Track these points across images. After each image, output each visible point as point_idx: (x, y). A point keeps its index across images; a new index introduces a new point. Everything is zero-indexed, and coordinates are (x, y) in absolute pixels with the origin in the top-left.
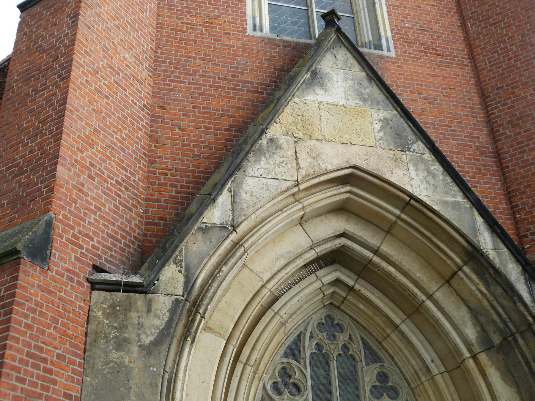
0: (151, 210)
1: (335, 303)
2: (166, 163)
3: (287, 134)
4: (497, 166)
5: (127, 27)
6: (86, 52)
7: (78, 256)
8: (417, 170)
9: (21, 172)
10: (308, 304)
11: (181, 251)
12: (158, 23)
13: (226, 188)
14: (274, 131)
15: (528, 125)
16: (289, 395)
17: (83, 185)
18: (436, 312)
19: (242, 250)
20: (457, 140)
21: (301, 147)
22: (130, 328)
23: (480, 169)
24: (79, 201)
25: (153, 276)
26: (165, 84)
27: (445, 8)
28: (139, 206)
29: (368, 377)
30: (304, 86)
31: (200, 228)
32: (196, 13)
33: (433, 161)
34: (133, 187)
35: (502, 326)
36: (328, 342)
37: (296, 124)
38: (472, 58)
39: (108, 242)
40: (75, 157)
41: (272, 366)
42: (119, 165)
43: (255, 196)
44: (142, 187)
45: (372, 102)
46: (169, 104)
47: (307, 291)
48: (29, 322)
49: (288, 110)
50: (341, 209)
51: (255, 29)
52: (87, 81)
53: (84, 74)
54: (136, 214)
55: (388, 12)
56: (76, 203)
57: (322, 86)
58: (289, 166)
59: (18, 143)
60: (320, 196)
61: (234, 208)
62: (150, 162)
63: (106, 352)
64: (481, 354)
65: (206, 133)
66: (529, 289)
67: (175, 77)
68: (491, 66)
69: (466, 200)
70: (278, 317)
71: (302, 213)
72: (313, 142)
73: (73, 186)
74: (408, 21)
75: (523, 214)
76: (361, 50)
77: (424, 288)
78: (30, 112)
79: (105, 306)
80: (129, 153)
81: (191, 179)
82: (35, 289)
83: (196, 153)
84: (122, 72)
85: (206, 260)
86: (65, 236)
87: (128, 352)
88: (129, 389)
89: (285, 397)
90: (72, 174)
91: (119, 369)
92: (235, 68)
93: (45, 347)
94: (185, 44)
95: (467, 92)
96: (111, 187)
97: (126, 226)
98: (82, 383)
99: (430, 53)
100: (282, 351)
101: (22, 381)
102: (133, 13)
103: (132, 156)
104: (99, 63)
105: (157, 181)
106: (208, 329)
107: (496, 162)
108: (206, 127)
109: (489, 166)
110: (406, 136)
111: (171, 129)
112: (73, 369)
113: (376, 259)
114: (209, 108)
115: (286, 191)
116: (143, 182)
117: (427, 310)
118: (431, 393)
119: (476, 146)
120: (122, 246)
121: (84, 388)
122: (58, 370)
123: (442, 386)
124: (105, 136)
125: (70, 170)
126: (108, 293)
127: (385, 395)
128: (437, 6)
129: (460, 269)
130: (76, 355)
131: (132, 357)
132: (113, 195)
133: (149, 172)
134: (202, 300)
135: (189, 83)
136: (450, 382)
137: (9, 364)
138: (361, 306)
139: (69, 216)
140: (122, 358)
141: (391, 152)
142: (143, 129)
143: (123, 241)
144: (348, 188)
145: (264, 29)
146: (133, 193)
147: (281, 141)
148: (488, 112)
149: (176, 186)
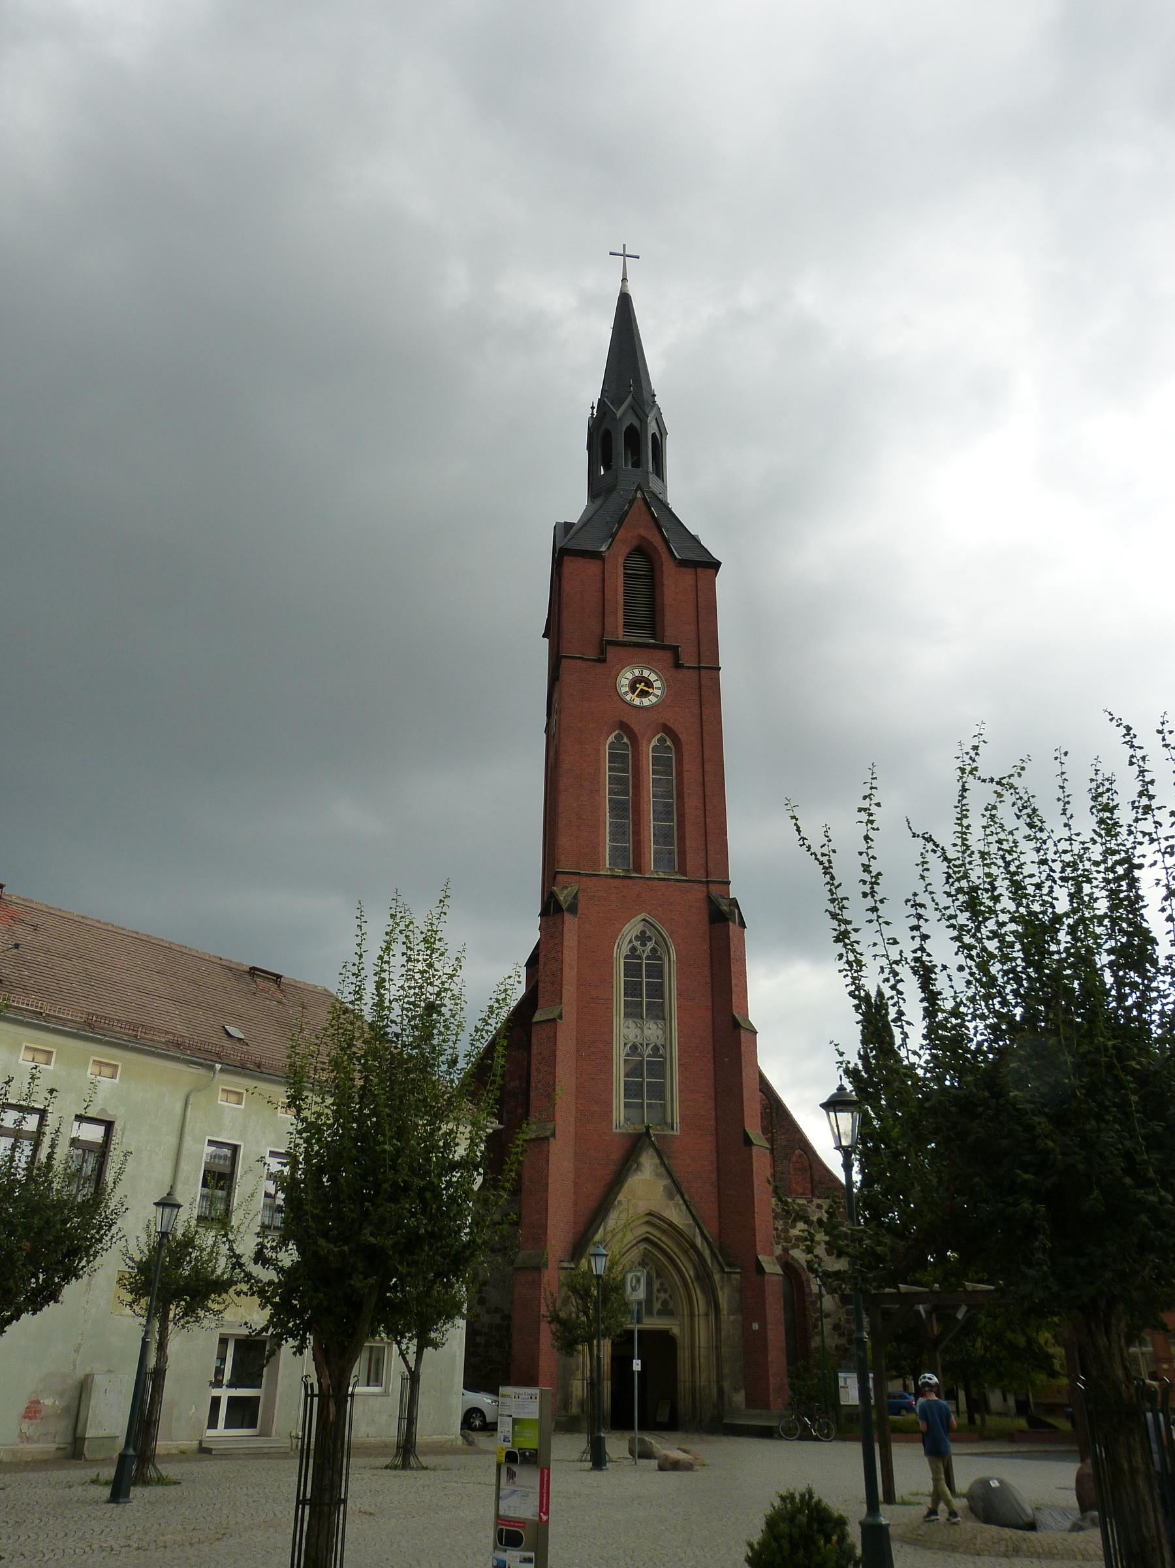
14: (620, 1197)
29: (656, 1286)
50: (647, 1223)
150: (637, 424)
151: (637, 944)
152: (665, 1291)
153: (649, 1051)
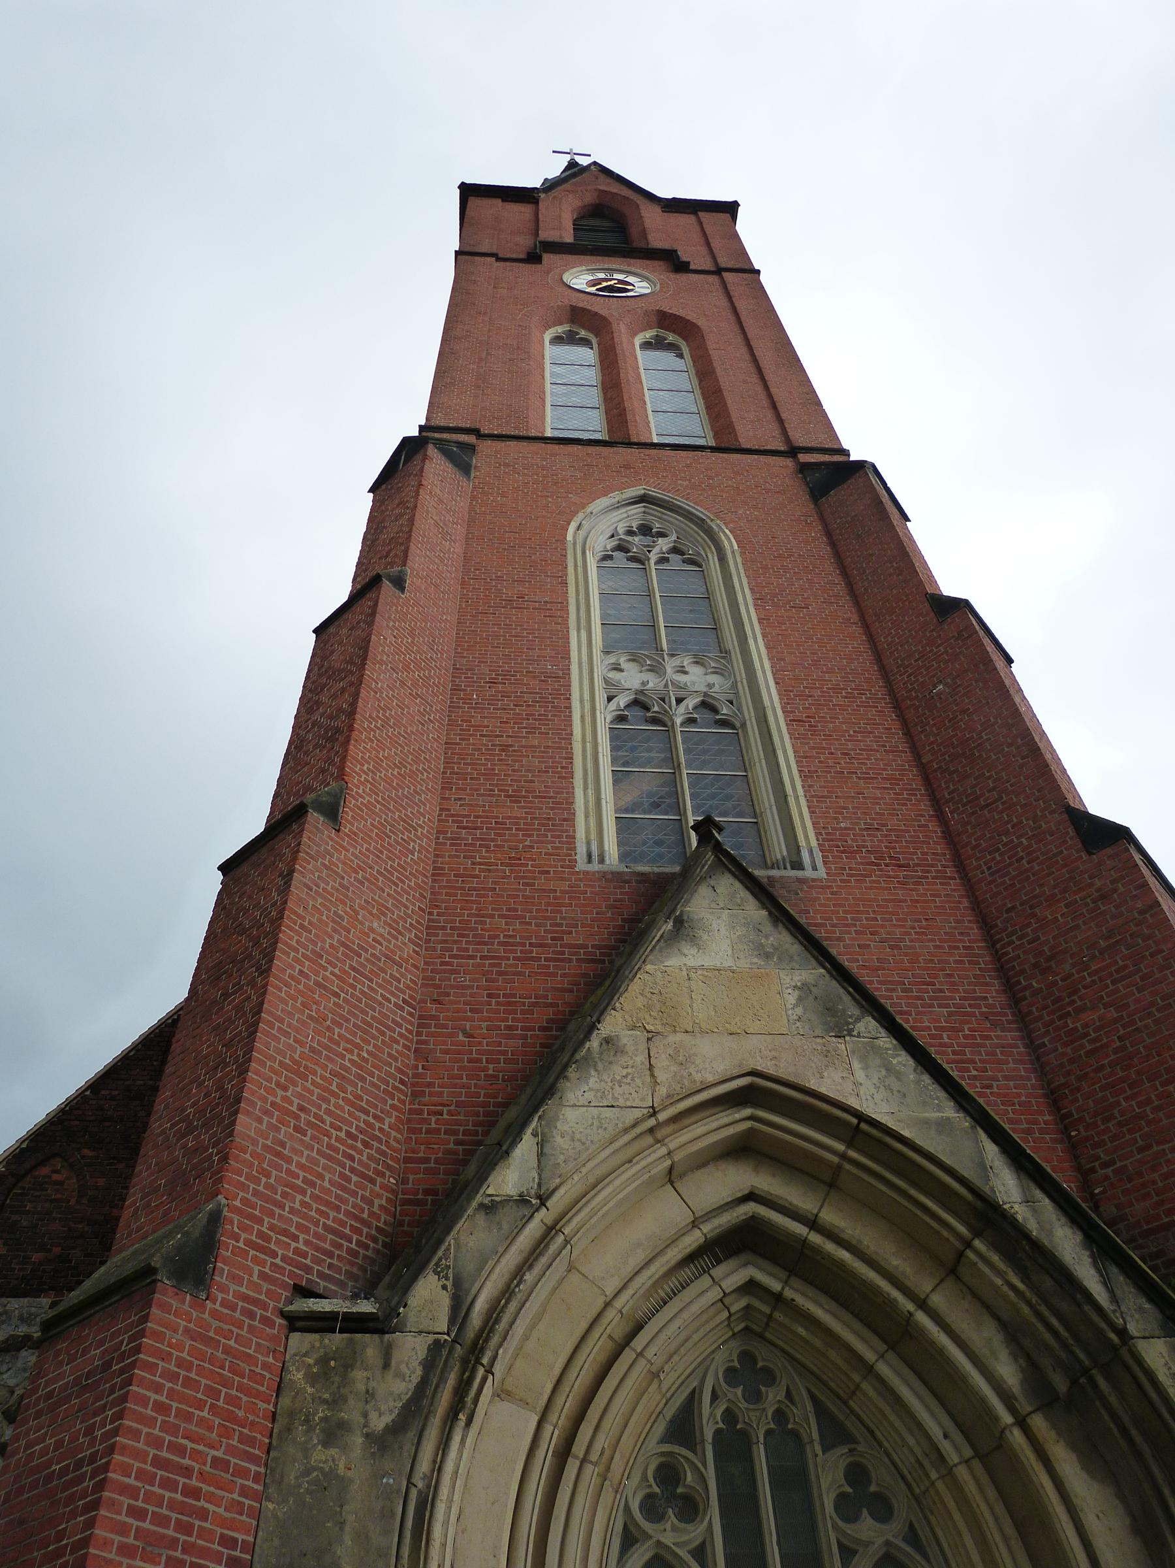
0: (411, 1177)
1: (754, 1327)
2: (441, 1094)
3: (633, 1028)
4: (1026, 1046)
5: (377, 880)
6: (302, 926)
7: (267, 1270)
8: (866, 1068)
9: (190, 1129)
10: (701, 1333)
11: (448, 1249)
12: (435, 868)
13: (529, 1131)
14: (612, 1024)
15: (1067, 967)
16: (675, 1521)
17: (283, 1145)
18: (936, 1334)
19: (560, 1239)
20: (947, 1006)
21: (658, 1046)
22: (351, 1402)
23: (994, 1054)
24: (274, 1172)
25: (396, 1299)
26: (442, 964)
27: (906, 789)
28: (388, 1173)
29: (828, 1477)
30: (662, 943)
31: (481, 1206)
32: (495, 846)
33: (895, 1049)
34: (380, 1141)
35: (1063, 1355)
36: (746, 1405)
37: (649, 1008)
38: (959, 863)
39: (325, 1241)
40: (271, 1098)
41: (639, 1460)
42: (352, 1105)
43: (579, 1140)
44: (395, 1139)
45: (779, 958)
46: (448, 995)
47: (696, 1308)
48: (163, 1399)
49: (635, 987)
51: (590, 860)
52: (301, 972)
53: (296, 960)
54: (382, 1187)
55: (809, 807)
56: (268, 1176)
57: (694, 940)
58: (638, 1081)
59: (192, 1082)
60: (699, 1129)
61: (543, 1164)
62: (415, 1095)
63: (306, 1451)
64: (1033, 1415)
65: (508, 1037)
66: (1101, 1275)
67: (459, 949)
68: (991, 874)
69: (961, 1115)
70: (642, 1362)
71: (669, 1162)
72: (679, 1037)
73: (266, 1148)
74: (844, 818)
75: (1082, 1130)
76: (758, 873)
77: (908, 1288)
78: (214, 1029)
79: (311, 1361)
80: (373, 1084)
81: (481, 1118)
82: (179, 1337)
83: (491, 1072)
84: (366, 951)
85: (490, 1263)
86: (244, 1236)
87: (345, 1449)
88: (342, 1524)
89: (668, 1526)
90: (264, 1127)
91: (329, 1484)
92: (557, 925)
93: (190, 1445)
94: (477, 896)
95: (957, 922)
96: (337, 1144)
97: (363, 1211)
98: (258, 1515)
99: (886, 865)
100: (660, 1429)
101: (140, 1514)
102: (389, 858)
103: (378, 1088)
104: (324, 941)
105: (424, 1127)
106: (502, 1394)
107: (1022, 1038)
108: (508, 1028)
109: (1011, 1046)
110: (844, 1011)
111: (451, 1035)
112: (242, 1486)
113: (815, 1238)
114: (514, 996)
115: (634, 1126)
116: (398, 1130)
117: (922, 1331)
118: (951, 1505)
119: (982, 1014)
120: (353, 1246)
121: (261, 1524)
122: (212, 1489)
123: (971, 1488)
124: (329, 1059)
125: (260, 1121)
126: (316, 1336)
127: (865, 1512)
128: (891, 789)
129: (968, 1245)
130: (254, 1459)
131: (350, 1460)
132: (340, 1157)
133: (411, 1111)
134: (487, 1340)
135: (482, 958)
136: (985, 1480)
137: (117, 1481)
138: (801, 1331)
139: (254, 1199)
140: (333, 1460)
141: (819, 1040)
142: (402, 1041)
143: (355, 1237)
144: (748, 1112)
145: (607, 859)
146: (378, 1151)
147: (624, 1041)
148: (997, 952)
149: (456, 1133)
152: (882, 1510)
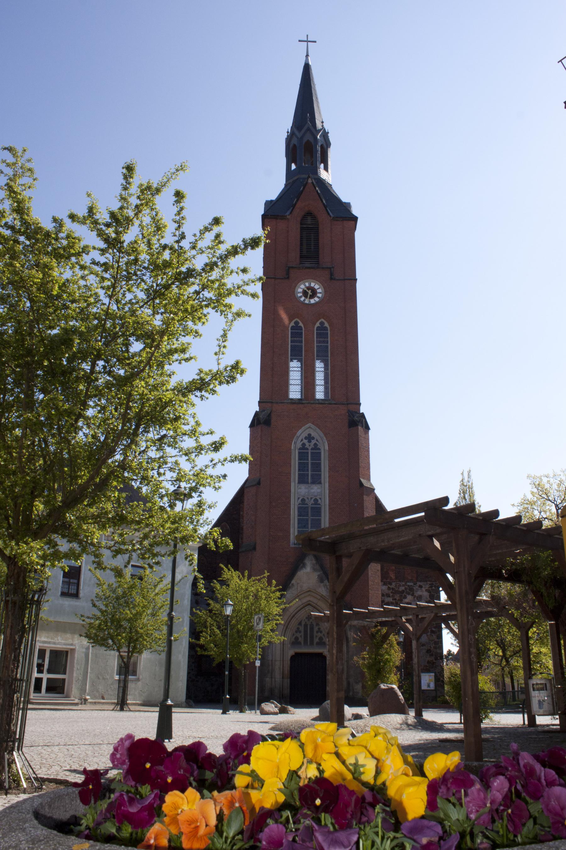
14: (293, 582)
150: (312, 140)
151: (305, 441)
152: (321, 632)
153: (312, 501)
